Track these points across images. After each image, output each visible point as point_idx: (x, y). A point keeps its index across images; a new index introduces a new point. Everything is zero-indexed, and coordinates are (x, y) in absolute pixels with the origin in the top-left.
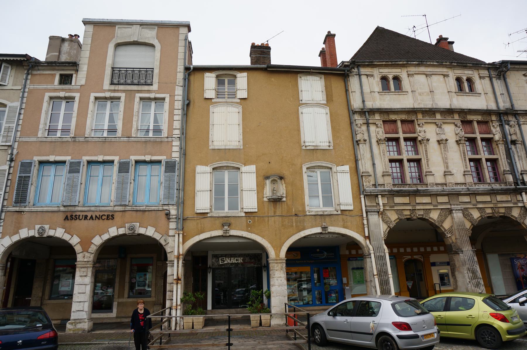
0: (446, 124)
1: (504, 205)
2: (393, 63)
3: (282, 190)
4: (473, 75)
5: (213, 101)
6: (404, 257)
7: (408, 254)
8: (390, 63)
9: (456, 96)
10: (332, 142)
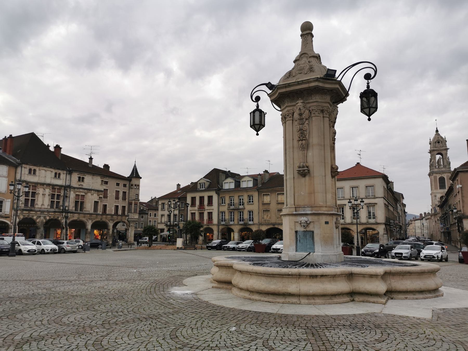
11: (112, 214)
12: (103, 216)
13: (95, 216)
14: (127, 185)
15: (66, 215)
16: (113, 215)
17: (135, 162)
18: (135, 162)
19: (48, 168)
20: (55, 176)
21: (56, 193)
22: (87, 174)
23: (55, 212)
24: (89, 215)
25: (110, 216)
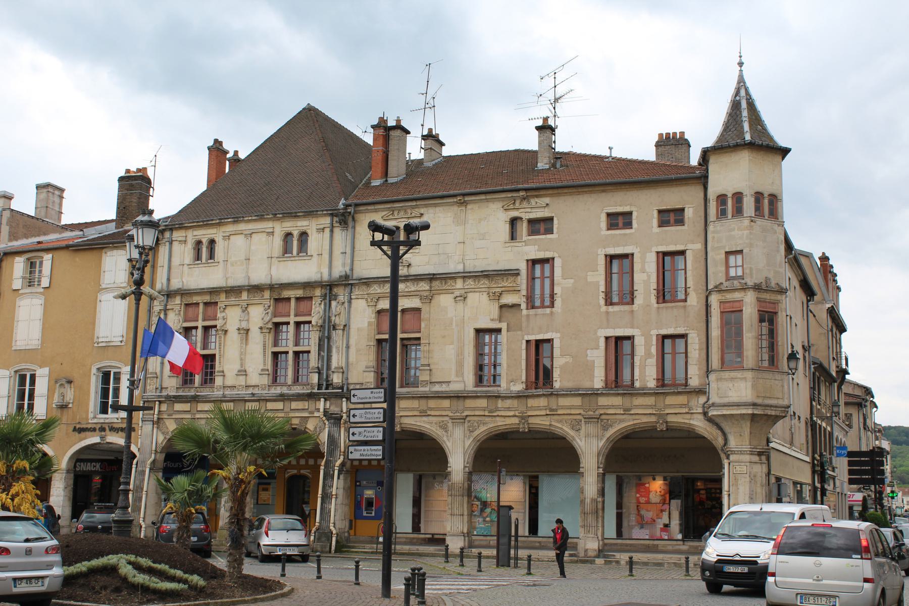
0: (253, 305)
1: (297, 414)
2: (205, 223)
3: (70, 394)
4: (308, 228)
5: (21, 292)
6: (289, 471)
7: (293, 467)
8: (202, 223)
9: (276, 262)
10: (125, 336)
11: (587, 385)
12: (531, 402)
13: (483, 403)
14: (689, 213)
15: (334, 409)
16: (594, 394)
17: (741, 64)
18: (741, 64)
19: (249, 221)
20: (287, 250)
21: (200, 324)
22: (426, 206)
23: (282, 398)
24: (446, 403)
25: (577, 401)
